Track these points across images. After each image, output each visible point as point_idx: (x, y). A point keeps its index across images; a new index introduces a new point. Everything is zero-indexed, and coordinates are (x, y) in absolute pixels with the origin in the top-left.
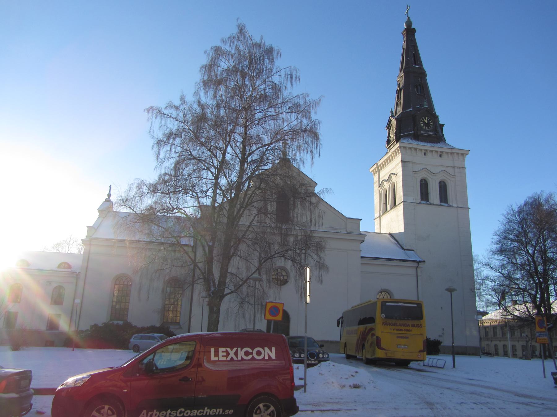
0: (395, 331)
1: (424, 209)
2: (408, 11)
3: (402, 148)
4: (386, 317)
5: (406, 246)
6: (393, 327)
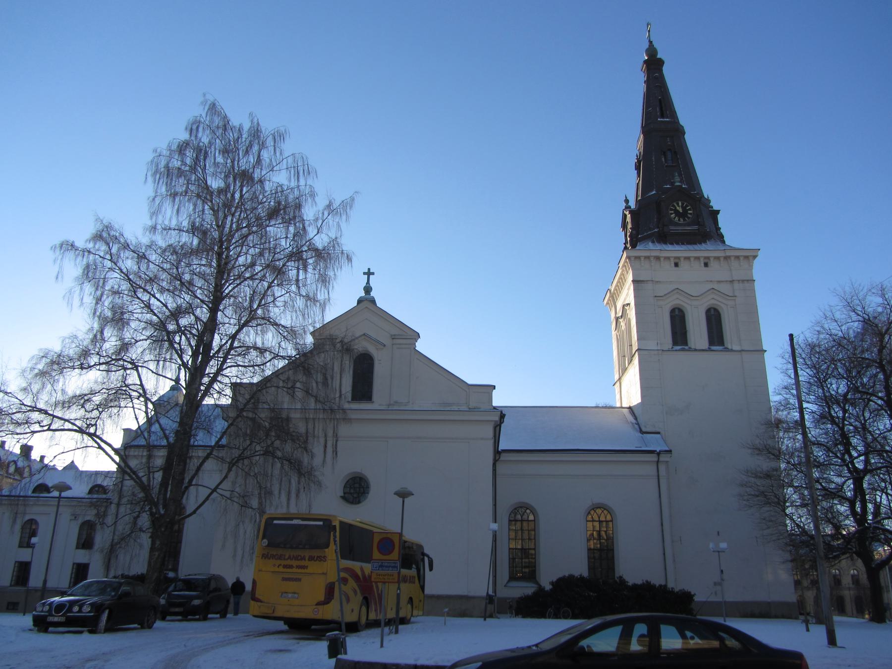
0: (281, 569)
1: (682, 357)
2: (649, 31)
3: (633, 259)
4: (268, 546)
5: (645, 427)
6: (278, 562)
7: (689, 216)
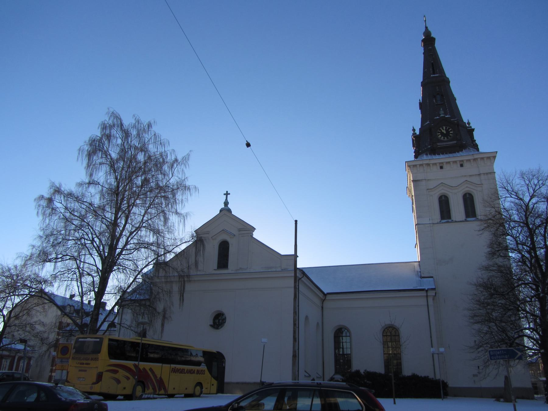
0: (79, 365)
1: (446, 227)
3: (412, 167)
5: (423, 274)
7: (451, 135)
